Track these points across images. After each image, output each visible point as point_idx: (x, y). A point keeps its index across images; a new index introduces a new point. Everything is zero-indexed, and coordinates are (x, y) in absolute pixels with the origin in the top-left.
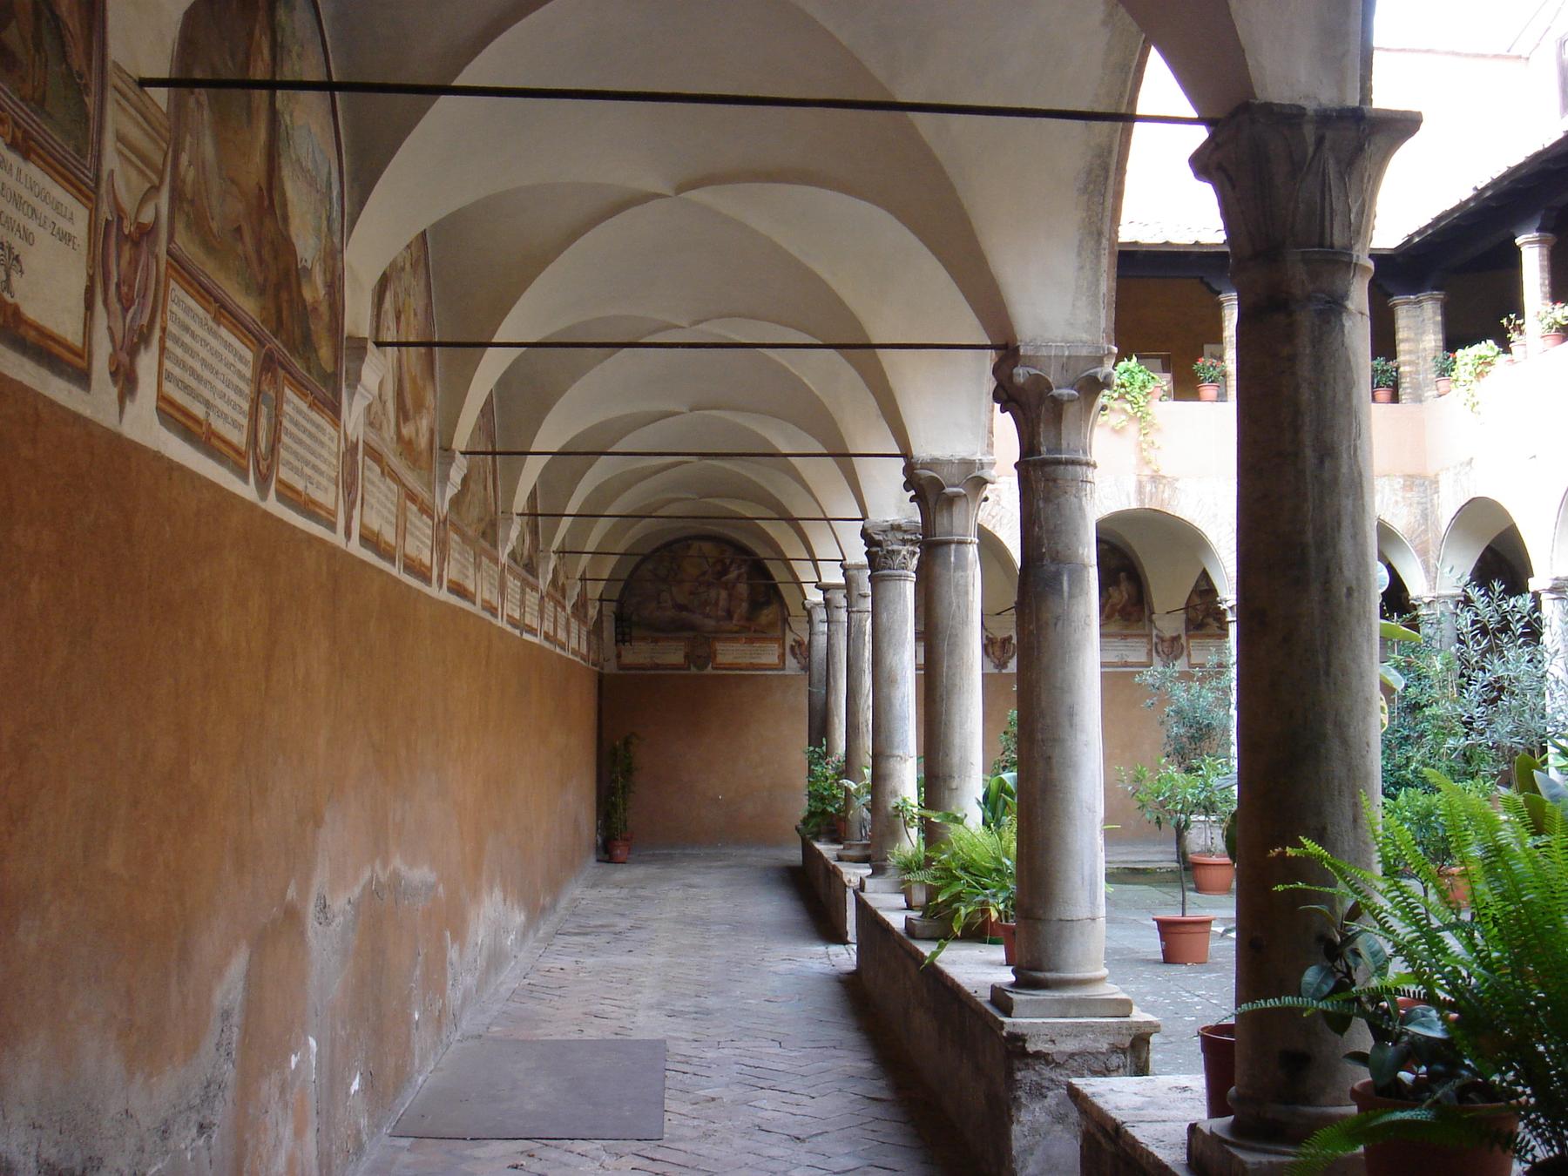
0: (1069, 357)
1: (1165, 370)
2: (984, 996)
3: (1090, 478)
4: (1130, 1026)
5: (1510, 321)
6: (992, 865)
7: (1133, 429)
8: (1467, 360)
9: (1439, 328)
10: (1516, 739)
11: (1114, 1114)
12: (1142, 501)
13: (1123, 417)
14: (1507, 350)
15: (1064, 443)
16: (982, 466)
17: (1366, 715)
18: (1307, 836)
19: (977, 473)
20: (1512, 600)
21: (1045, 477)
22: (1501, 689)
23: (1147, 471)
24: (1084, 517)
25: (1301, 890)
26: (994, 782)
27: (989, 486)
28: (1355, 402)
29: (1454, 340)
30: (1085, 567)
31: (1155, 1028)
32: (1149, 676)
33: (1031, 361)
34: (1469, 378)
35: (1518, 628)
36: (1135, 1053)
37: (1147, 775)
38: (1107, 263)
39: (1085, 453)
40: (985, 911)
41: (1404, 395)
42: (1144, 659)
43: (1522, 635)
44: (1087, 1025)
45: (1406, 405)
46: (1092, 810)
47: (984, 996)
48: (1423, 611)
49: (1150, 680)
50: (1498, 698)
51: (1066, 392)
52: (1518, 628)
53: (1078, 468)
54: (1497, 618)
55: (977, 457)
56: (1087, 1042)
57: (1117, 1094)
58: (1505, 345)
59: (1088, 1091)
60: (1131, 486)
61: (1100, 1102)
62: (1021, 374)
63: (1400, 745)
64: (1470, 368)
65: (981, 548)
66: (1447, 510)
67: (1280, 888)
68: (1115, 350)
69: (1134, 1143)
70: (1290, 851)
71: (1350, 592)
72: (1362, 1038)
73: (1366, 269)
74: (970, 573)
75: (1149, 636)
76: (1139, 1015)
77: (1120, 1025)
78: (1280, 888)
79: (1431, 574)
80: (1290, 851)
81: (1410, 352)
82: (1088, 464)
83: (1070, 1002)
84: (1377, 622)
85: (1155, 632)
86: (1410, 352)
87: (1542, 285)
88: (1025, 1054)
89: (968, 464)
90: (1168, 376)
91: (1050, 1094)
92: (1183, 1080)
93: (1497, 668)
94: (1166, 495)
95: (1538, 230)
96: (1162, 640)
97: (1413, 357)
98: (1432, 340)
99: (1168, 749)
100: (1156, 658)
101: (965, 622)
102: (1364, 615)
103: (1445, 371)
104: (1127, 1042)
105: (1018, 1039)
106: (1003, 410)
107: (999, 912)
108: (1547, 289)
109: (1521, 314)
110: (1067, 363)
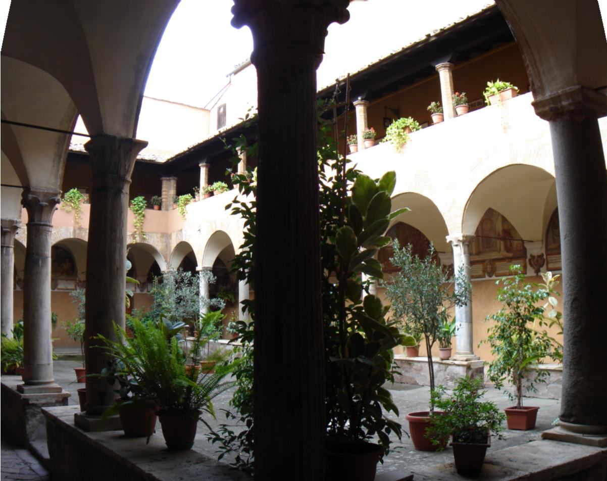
0: (47, 193)
1: (87, 193)
2: (15, 389)
3: (50, 230)
4: (62, 395)
5: (195, 188)
6: (16, 349)
7: (74, 212)
8: (182, 199)
9: (175, 188)
10: (184, 314)
11: (54, 415)
12: (75, 236)
13: (71, 208)
14: (194, 197)
15: (43, 218)
16: (17, 222)
17: (121, 302)
18: (100, 334)
19: (15, 225)
20: (185, 273)
21: (36, 229)
22: (181, 300)
23: (77, 226)
24: (47, 242)
25: (96, 348)
26: (17, 325)
27: (19, 229)
28: (122, 217)
29: (179, 193)
30: (47, 257)
31: (70, 395)
32: (74, 293)
33: (34, 193)
34: (182, 205)
35: (186, 281)
36: (64, 401)
37: (71, 324)
38: (64, 157)
39: (49, 222)
40: (15, 365)
41: (163, 208)
42: (73, 287)
43: (187, 283)
44: (48, 395)
45: (163, 211)
46: (48, 332)
47: (15, 389)
48: (164, 276)
49: (74, 294)
50: (180, 302)
51: (45, 203)
52: (186, 281)
53: (47, 227)
54: (180, 278)
55: (15, 219)
56: (48, 400)
57: (57, 411)
58: (194, 197)
59: (47, 410)
60: (72, 231)
61: (51, 412)
62: (30, 196)
63: (156, 317)
64: (183, 202)
65: (15, 249)
66: (174, 244)
67: (91, 347)
68: (61, 192)
69: (60, 421)
70: (95, 337)
71: (118, 269)
72: (118, 386)
73: (129, 182)
74: (10, 257)
75: (75, 280)
76: (64, 392)
77: (58, 395)
78: (91, 347)
79: (169, 266)
80: (95, 337)
81: (166, 195)
82: (50, 226)
83: (43, 389)
84: (125, 278)
85: (77, 279)
86: (166, 195)
87: (205, 179)
88: (29, 404)
89: (12, 222)
90: (87, 195)
91: (38, 416)
92: (76, 406)
93: (180, 293)
94: (83, 234)
95: (206, 163)
96: (80, 281)
97: (166, 197)
98: (172, 192)
99: (81, 317)
100: (78, 288)
101: (566, 237)
102: (121, 275)
103: (176, 201)
104: (61, 400)
105: (26, 401)
106: (24, 207)
107: (19, 364)
108: (207, 180)
109: (199, 187)
110: (46, 195)
